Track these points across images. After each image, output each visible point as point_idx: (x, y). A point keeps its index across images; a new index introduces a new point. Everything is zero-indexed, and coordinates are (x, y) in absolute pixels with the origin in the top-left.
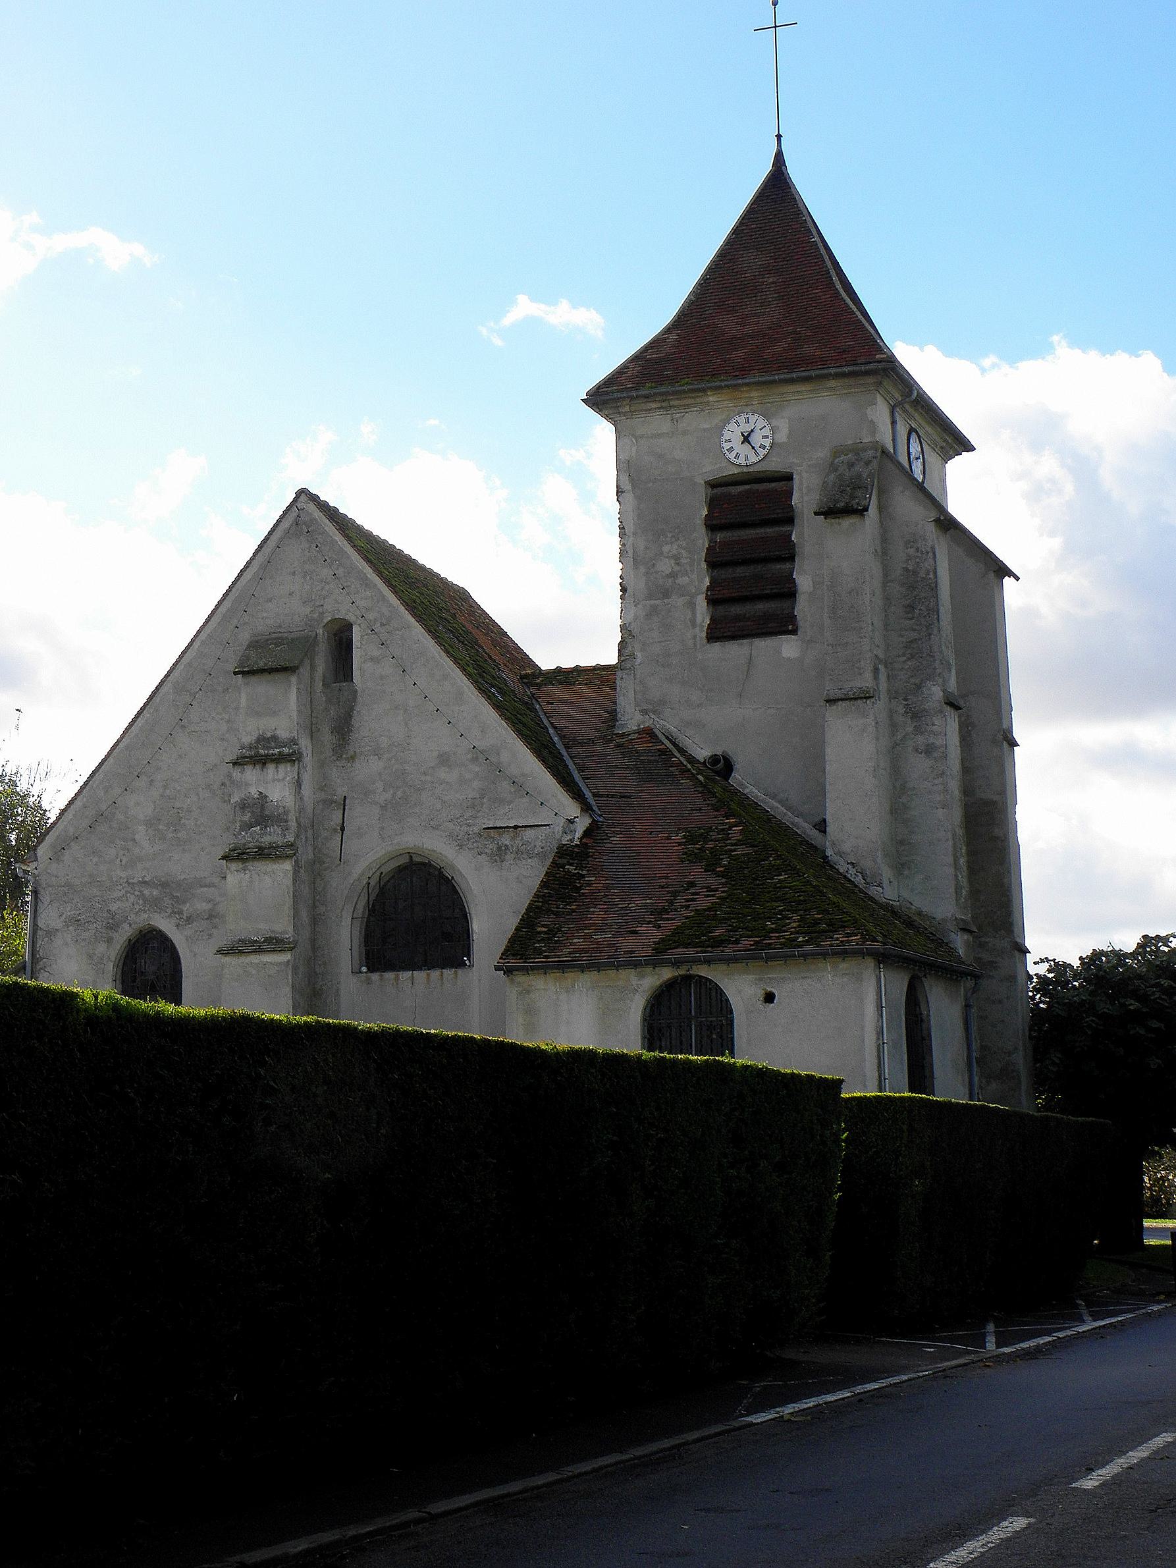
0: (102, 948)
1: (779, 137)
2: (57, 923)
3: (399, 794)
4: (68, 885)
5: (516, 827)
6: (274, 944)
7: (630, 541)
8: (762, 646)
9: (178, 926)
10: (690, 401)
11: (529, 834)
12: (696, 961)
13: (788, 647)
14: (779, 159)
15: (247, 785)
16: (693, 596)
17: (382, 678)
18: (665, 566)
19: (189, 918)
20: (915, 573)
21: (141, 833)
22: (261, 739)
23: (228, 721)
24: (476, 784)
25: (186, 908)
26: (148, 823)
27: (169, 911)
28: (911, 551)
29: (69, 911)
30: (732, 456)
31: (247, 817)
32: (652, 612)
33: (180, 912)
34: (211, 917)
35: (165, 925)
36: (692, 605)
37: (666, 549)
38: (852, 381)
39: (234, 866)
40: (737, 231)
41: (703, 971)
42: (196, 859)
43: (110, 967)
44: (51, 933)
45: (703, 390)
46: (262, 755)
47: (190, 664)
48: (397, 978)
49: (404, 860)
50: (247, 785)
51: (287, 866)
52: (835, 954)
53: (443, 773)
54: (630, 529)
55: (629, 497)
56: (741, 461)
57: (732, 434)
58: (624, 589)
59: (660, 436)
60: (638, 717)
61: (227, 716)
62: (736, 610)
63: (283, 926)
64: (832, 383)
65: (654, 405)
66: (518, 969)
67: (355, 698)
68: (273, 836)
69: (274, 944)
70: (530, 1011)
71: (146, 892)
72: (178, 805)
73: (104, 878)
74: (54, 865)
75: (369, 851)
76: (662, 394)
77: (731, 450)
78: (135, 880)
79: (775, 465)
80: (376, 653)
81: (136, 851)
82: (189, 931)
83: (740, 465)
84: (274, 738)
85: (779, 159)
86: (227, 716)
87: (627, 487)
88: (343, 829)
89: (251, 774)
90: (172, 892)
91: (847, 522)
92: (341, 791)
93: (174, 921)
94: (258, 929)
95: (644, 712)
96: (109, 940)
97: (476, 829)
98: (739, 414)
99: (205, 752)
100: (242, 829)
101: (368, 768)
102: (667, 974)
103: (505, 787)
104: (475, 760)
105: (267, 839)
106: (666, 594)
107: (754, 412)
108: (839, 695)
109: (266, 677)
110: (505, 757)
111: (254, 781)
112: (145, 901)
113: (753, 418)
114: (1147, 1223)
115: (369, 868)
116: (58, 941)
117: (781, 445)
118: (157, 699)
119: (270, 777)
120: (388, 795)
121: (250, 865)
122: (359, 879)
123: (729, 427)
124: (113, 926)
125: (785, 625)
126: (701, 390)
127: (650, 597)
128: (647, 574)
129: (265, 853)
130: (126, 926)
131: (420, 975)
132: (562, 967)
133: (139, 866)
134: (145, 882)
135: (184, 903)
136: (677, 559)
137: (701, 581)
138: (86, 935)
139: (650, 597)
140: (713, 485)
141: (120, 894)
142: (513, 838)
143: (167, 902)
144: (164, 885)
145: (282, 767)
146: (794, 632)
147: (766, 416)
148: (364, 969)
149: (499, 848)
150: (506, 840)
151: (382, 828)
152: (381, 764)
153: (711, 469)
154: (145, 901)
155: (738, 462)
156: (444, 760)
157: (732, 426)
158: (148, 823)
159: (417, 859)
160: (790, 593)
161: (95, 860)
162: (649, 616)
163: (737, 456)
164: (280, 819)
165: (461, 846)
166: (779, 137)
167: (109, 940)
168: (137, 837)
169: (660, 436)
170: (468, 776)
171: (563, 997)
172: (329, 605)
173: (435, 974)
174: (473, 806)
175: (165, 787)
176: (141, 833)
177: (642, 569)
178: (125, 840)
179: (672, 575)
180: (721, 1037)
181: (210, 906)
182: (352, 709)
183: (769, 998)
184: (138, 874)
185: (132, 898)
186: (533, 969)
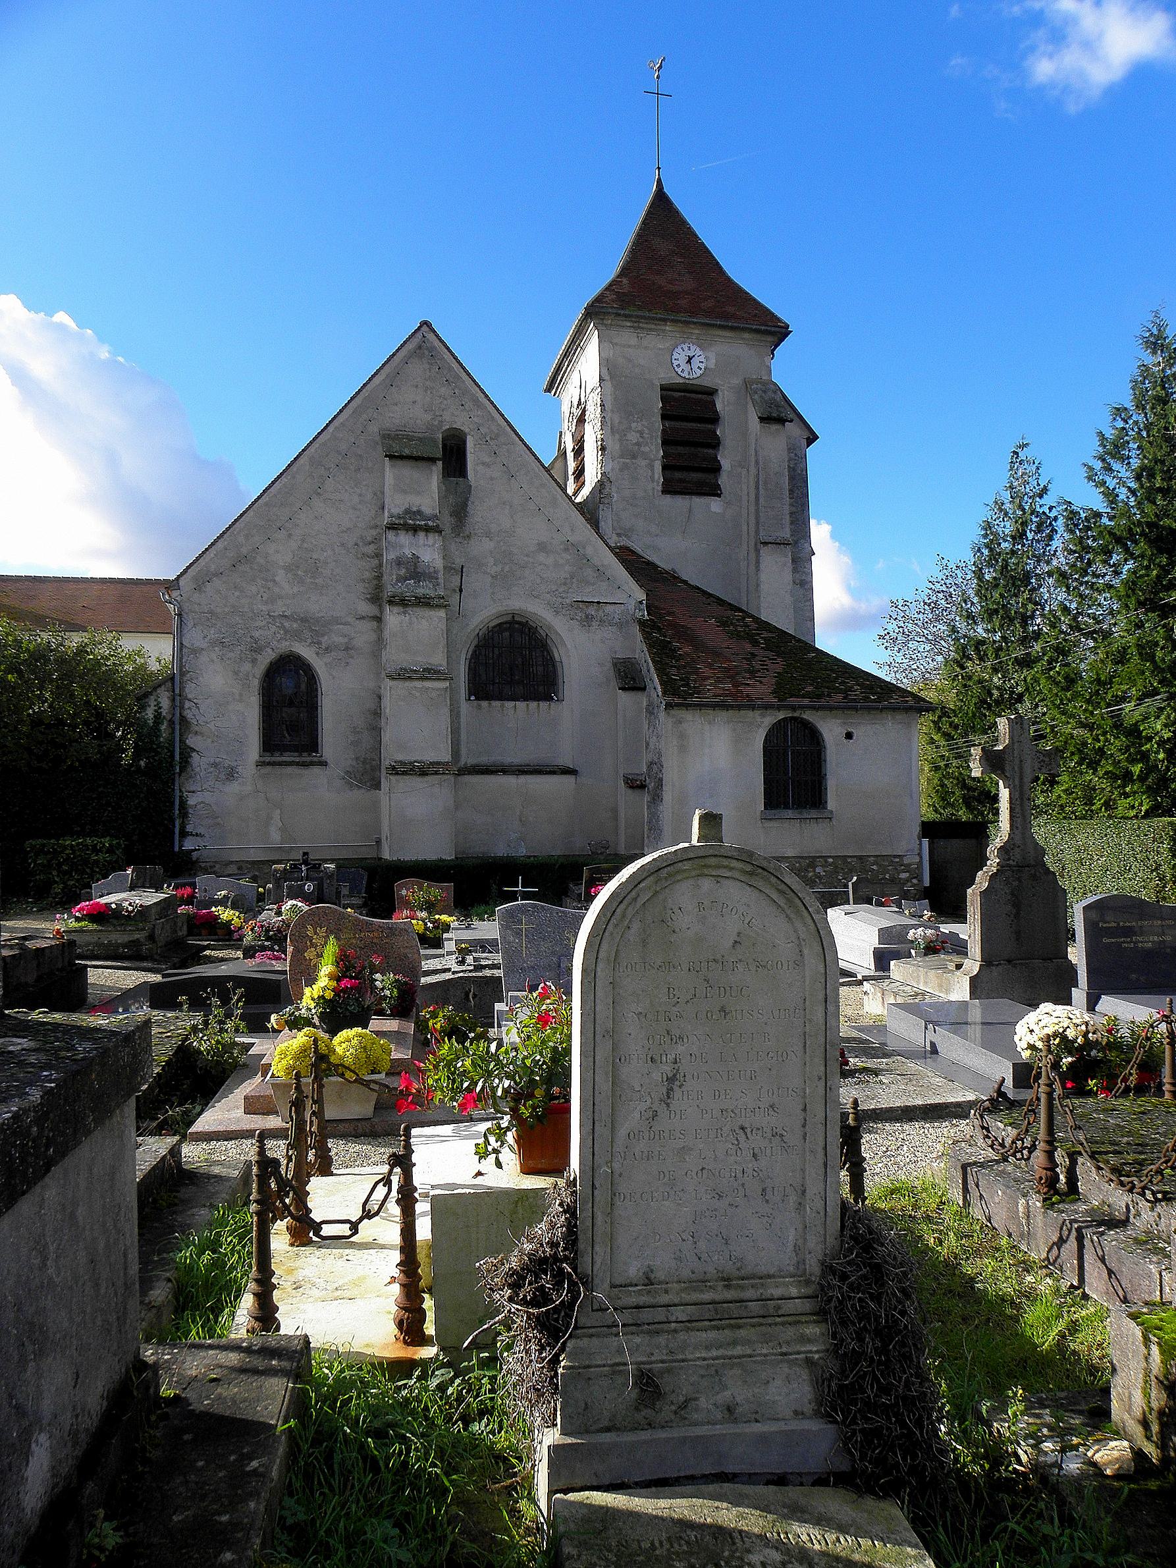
0: (247, 667)
2: (200, 643)
3: (507, 568)
4: (211, 612)
5: (598, 603)
6: (429, 674)
7: (608, 416)
8: (698, 501)
9: (317, 654)
10: (653, 326)
11: (609, 608)
12: (802, 707)
15: (402, 546)
16: (652, 461)
17: (492, 479)
18: (633, 437)
19: (327, 649)
20: (794, 469)
21: (281, 576)
22: (408, 511)
23: (360, 495)
25: (324, 639)
26: (288, 569)
27: (309, 641)
29: (212, 634)
31: (403, 572)
32: (624, 468)
33: (319, 643)
34: (347, 649)
35: (306, 652)
36: (652, 467)
37: (634, 425)
38: (758, 336)
39: (396, 609)
40: (684, 222)
41: (808, 716)
42: (341, 600)
43: (256, 683)
44: (196, 652)
45: (665, 320)
46: (411, 524)
47: (324, 444)
48: (503, 706)
49: (509, 618)
50: (402, 546)
51: (442, 613)
53: (541, 557)
54: (608, 406)
55: (608, 384)
56: (685, 375)
57: (680, 356)
58: (603, 449)
59: (629, 346)
60: (615, 538)
61: (358, 491)
62: (678, 475)
63: (438, 659)
64: (746, 335)
66: (678, 705)
67: (470, 492)
68: (425, 589)
69: (429, 674)
70: (682, 736)
71: (287, 624)
72: (315, 556)
74: (196, 595)
75: (484, 608)
76: (637, 316)
77: (678, 366)
79: (707, 382)
80: (487, 460)
81: (276, 590)
82: (328, 659)
84: (419, 512)
86: (358, 491)
87: (607, 377)
88: (461, 591)
89: (404, 538)
90: (313, 627)
91: (774, 427)
92: (459, 561)
93: (313, 649)
94: (418, 661)
95: (619, 535)
96: (254, 661)
97: (568, 601)
99: (340, 518)
100: (398, 580)
101: (481, 547)
102: (781, 715)
103: (589, 573)
104: (566, 550)
105: (420, 591)
106: (634, 457)
109: (413, 463)
110: (589, 551)
111: (406, 545)
112: (286, 632)
113: (693, 348)
114: (177, 849)
115: (482, 622)
116: (204, 658)
117: (710, 370)
118: (294, 468)
119: (421, 542)
120: (499, 569)
121: (409, 610)
122: (474, 630)
124: (258, 650)
125: (714, 491)
126: (660, 319)
127: (622, 456)
128: (620, 440)
129: (424, 602)
130: (269, 650)
131: (521, 705)
132: (700, 706)
133: (280, 602)
135: (323, 635)
136: (641, 433)
137: (658, 451)
139: (622, 456)
140: (663, 388)
141: (262, 624)
142: (598, 610)
143: (307, 634)
144: (304, 620)
145: (431, 535)
146: (719, 496)
147: (702, 349)
148: (473, 698)
149: (587, 617)
150: (592, 611)
151: (493, 593)
152: (492, 544)
153: (665, 376)
154: (286, 632)
156: (542, 547)
157: (679, 350)
158: (288, 569)
160: (716, 469)
161: (237, 594)
162: (621, 470)
164: (431, 576)
165: (557, 613)
167: (254, 661)
168: (277, 579)
169: (629, 346)
170: (561, 561)
171: (707, 727)
172: (447, 416)
173: (533, 705)
174: (565, 584)
175: (303, 541)
176: (281, 576)
177: (617, 436)
178: (266, 580)
179: (638, 444)
181: (346, 640)
182: (467, 499)
183: (849, 736)
184: (279, 608)
185: (274, 629)
186: (690, 705)
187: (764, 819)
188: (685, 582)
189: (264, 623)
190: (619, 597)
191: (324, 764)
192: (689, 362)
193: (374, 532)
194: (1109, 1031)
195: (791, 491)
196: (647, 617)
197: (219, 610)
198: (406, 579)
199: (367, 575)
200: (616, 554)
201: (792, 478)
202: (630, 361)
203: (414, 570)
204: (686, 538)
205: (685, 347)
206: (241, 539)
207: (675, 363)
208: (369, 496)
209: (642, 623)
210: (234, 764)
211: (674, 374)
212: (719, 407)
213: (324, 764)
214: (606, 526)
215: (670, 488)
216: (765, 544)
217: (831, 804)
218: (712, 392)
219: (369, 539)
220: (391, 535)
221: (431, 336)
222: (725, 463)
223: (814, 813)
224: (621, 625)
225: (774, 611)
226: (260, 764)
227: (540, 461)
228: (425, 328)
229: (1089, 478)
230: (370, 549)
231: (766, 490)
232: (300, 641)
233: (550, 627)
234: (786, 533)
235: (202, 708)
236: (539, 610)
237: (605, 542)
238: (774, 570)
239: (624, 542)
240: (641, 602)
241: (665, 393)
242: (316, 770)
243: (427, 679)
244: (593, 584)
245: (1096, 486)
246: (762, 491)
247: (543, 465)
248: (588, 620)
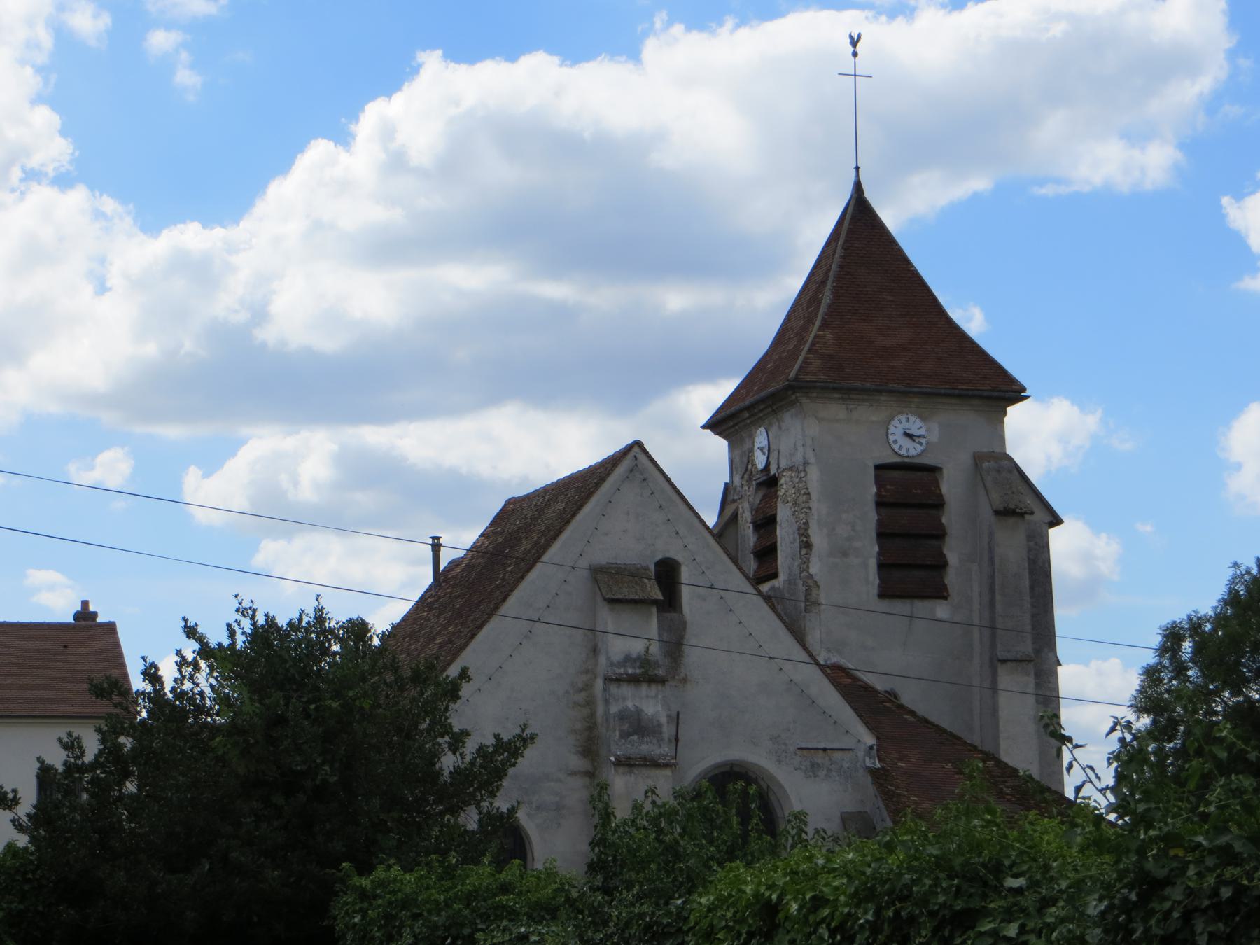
1: (857, 168)
5: (825, 750)
13: (941, 610)
14: (858, 187)
15: (624, 699)
28: (1032, 544)
30: (896, 447)
31: (626, 727)
39: (621, 770)
49: (728, 769)
56: (903, 452)
57: (897, 429)
67: (684, 629)
68: (647, 748)
77: (895, 442)
83: (903, 456)
85: (858, 187)
88: (677, 740)
89: (626, 690)
91: (1011, 521)
98: (901, 413)
106: (845, 554)
107: (913, 414)
108: (1009, 656)
123: (893, 423)
125: (940, 593)
145: (654, 687)
146: (945, 598)
149: (813, 765)
150: (819, 758)
155: (901, 453)
157: (895, 422)
159: (736, 769)
163: (901, 448)
165: (780, 762)
166: (857, 168)
180: (709, 910)
188: (913, 713)
190: (846, 742)
193: (585, 678)
195: (1032, 588)
196: (878, 765)
198: (630, 734)
199: (579, 726)
200: (827, 675)
201: (1032, 572)
203: (638, 726)
204: (905, 651)
205: (903, 418)
207: (892, 438)
209: (872, 772)
211: (890, 452)
212: (944, 489)
214: (814, 637)
215: (883, 595)
216: (1004, 661)
218: (933, 470)
219: (580, 685)
220: (613, 688)
221: (642, 457)
222: (953, 558)
225: (1019, 754)
227: (702, 521)
228: (636, 449)
230: (581, 697)
233: (772, 778)
234: (1027, 647)
236: (759, 758)
237: (740, 569)
238: (1015, 707)
239: (835, 659)
240: (871, 748)
246: (998, 597)
247: (707, 527)
248: (814, 768)
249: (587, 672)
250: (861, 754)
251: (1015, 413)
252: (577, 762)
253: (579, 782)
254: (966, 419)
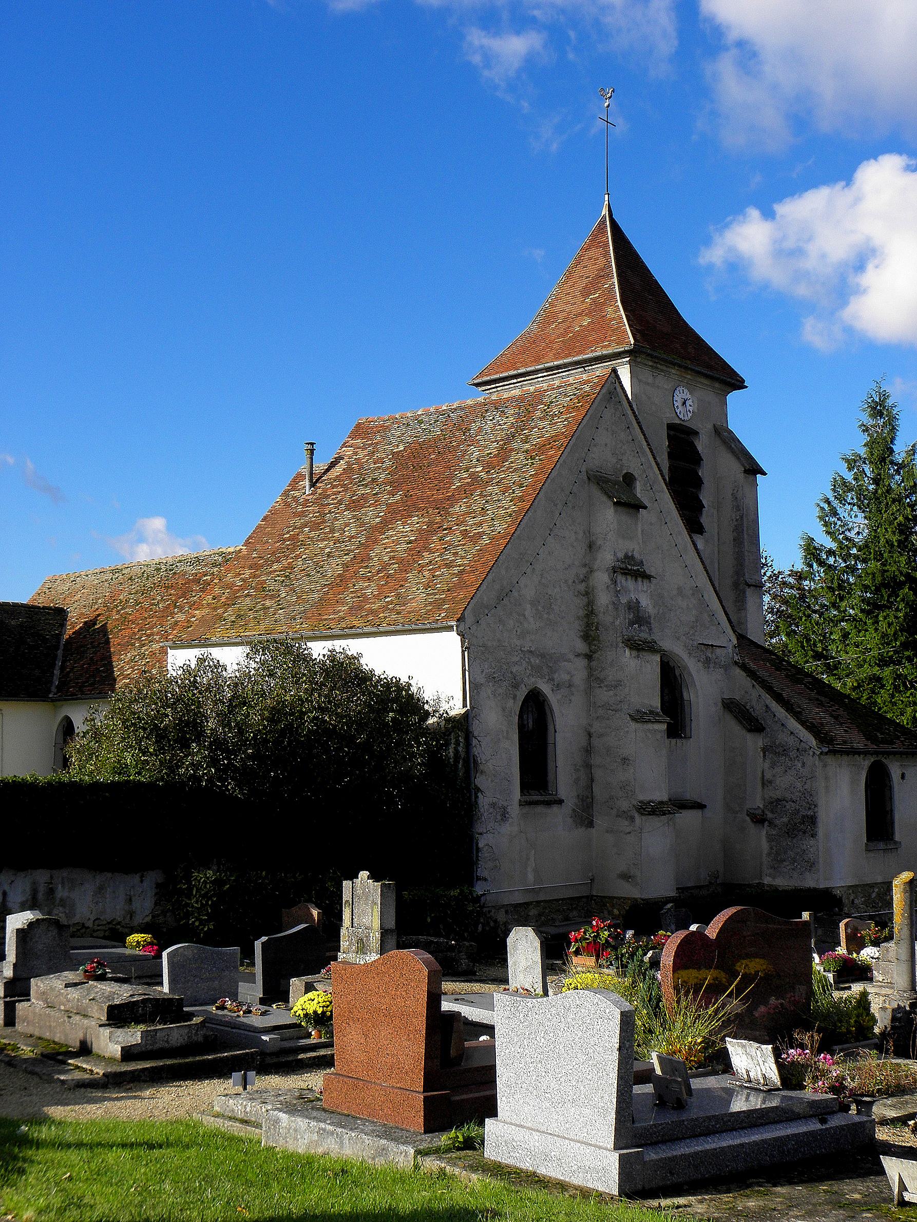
0: (510, 703)
4: (484, 646)
5: (712, 646)
10: (664, 368)
11: (718, 651)
24: (694, 612)
27: (547, 677)
33: (553, 680)
34: (570, 686)
35: (545, 688)
52: (901, 753)
64: (717, 385)
65: (650, 364)
70: (827, 778)
73: (506, 644)
78: (525, 649)
90: (547, 662)
96: (515, 698)
121: (642, 654)
124: (516, 686)
134: (531, 652)
138: (500, 691)
141: (517, 659)
143: (545, 670)
144: (542, 656)
153: (668, 417)
167: (515, 698)
168: (526, 613)
187: (868, 850)
189: (518, 658)
191: (560, 802)
192: (684, 403)
194: (303, 1009)
197: (490, 644)
202: (649, 398)
206: (503, 572)
208: (581, 534)
210: (505, 804)
211: (674, 414)
213: (560, 802)
216: (749, 586)
217: (897, 837)
223: (881, 845)
224: (726, 668)
226: (521, 804)
229: (821, 518)
230: (582, 587)
231: (748, 535)
232: (542, 677)
233: (686, 667)
235: (483, 744)
241: (672, 433)
242: (555, 808)
243: (649, 721)
244: (708, 628)
245: (824, 526)
249: (585, 565)
250: (730, 650)
251: (733, 397)
252: (581, 646)
253: (581, 663)
254: (708, 394)
